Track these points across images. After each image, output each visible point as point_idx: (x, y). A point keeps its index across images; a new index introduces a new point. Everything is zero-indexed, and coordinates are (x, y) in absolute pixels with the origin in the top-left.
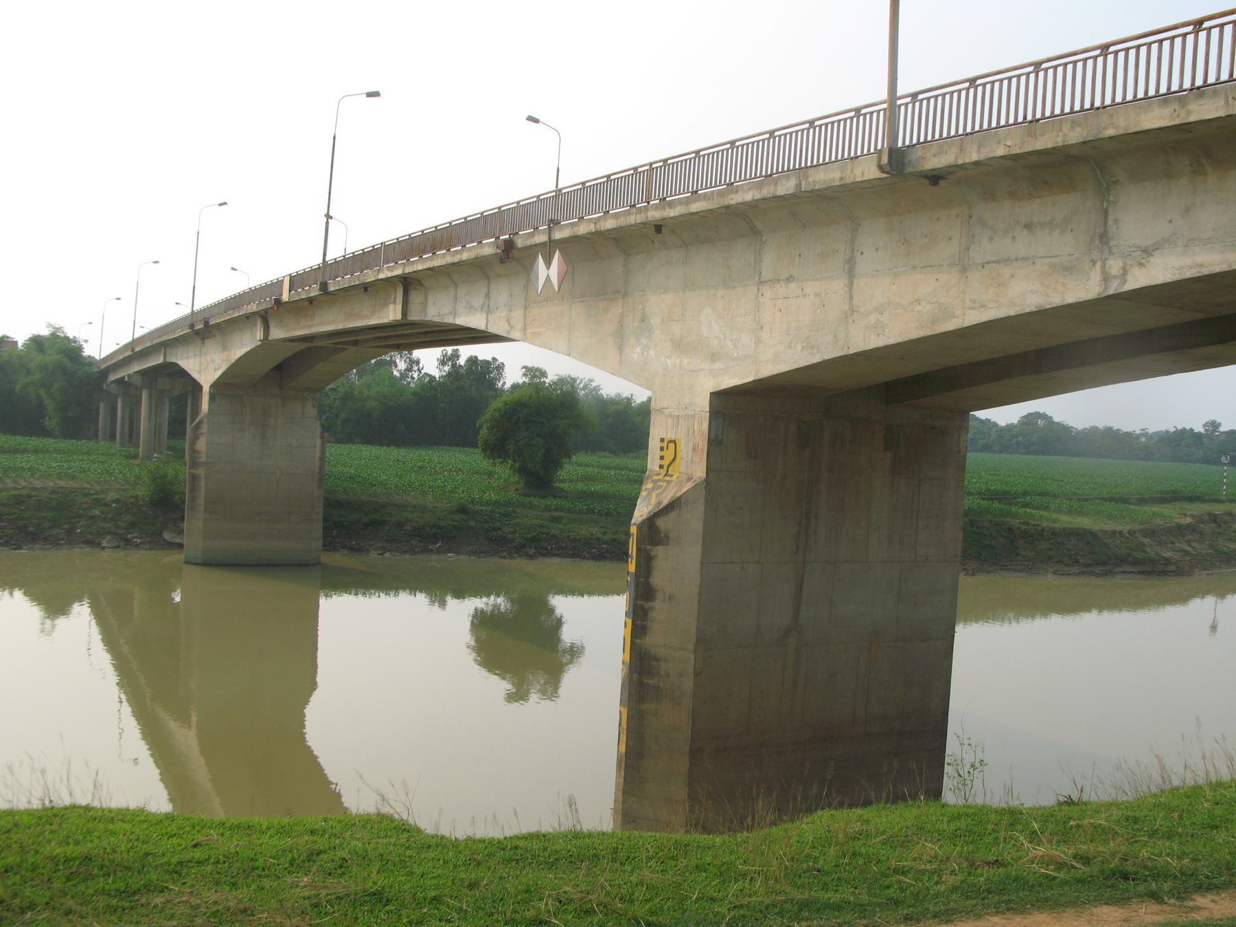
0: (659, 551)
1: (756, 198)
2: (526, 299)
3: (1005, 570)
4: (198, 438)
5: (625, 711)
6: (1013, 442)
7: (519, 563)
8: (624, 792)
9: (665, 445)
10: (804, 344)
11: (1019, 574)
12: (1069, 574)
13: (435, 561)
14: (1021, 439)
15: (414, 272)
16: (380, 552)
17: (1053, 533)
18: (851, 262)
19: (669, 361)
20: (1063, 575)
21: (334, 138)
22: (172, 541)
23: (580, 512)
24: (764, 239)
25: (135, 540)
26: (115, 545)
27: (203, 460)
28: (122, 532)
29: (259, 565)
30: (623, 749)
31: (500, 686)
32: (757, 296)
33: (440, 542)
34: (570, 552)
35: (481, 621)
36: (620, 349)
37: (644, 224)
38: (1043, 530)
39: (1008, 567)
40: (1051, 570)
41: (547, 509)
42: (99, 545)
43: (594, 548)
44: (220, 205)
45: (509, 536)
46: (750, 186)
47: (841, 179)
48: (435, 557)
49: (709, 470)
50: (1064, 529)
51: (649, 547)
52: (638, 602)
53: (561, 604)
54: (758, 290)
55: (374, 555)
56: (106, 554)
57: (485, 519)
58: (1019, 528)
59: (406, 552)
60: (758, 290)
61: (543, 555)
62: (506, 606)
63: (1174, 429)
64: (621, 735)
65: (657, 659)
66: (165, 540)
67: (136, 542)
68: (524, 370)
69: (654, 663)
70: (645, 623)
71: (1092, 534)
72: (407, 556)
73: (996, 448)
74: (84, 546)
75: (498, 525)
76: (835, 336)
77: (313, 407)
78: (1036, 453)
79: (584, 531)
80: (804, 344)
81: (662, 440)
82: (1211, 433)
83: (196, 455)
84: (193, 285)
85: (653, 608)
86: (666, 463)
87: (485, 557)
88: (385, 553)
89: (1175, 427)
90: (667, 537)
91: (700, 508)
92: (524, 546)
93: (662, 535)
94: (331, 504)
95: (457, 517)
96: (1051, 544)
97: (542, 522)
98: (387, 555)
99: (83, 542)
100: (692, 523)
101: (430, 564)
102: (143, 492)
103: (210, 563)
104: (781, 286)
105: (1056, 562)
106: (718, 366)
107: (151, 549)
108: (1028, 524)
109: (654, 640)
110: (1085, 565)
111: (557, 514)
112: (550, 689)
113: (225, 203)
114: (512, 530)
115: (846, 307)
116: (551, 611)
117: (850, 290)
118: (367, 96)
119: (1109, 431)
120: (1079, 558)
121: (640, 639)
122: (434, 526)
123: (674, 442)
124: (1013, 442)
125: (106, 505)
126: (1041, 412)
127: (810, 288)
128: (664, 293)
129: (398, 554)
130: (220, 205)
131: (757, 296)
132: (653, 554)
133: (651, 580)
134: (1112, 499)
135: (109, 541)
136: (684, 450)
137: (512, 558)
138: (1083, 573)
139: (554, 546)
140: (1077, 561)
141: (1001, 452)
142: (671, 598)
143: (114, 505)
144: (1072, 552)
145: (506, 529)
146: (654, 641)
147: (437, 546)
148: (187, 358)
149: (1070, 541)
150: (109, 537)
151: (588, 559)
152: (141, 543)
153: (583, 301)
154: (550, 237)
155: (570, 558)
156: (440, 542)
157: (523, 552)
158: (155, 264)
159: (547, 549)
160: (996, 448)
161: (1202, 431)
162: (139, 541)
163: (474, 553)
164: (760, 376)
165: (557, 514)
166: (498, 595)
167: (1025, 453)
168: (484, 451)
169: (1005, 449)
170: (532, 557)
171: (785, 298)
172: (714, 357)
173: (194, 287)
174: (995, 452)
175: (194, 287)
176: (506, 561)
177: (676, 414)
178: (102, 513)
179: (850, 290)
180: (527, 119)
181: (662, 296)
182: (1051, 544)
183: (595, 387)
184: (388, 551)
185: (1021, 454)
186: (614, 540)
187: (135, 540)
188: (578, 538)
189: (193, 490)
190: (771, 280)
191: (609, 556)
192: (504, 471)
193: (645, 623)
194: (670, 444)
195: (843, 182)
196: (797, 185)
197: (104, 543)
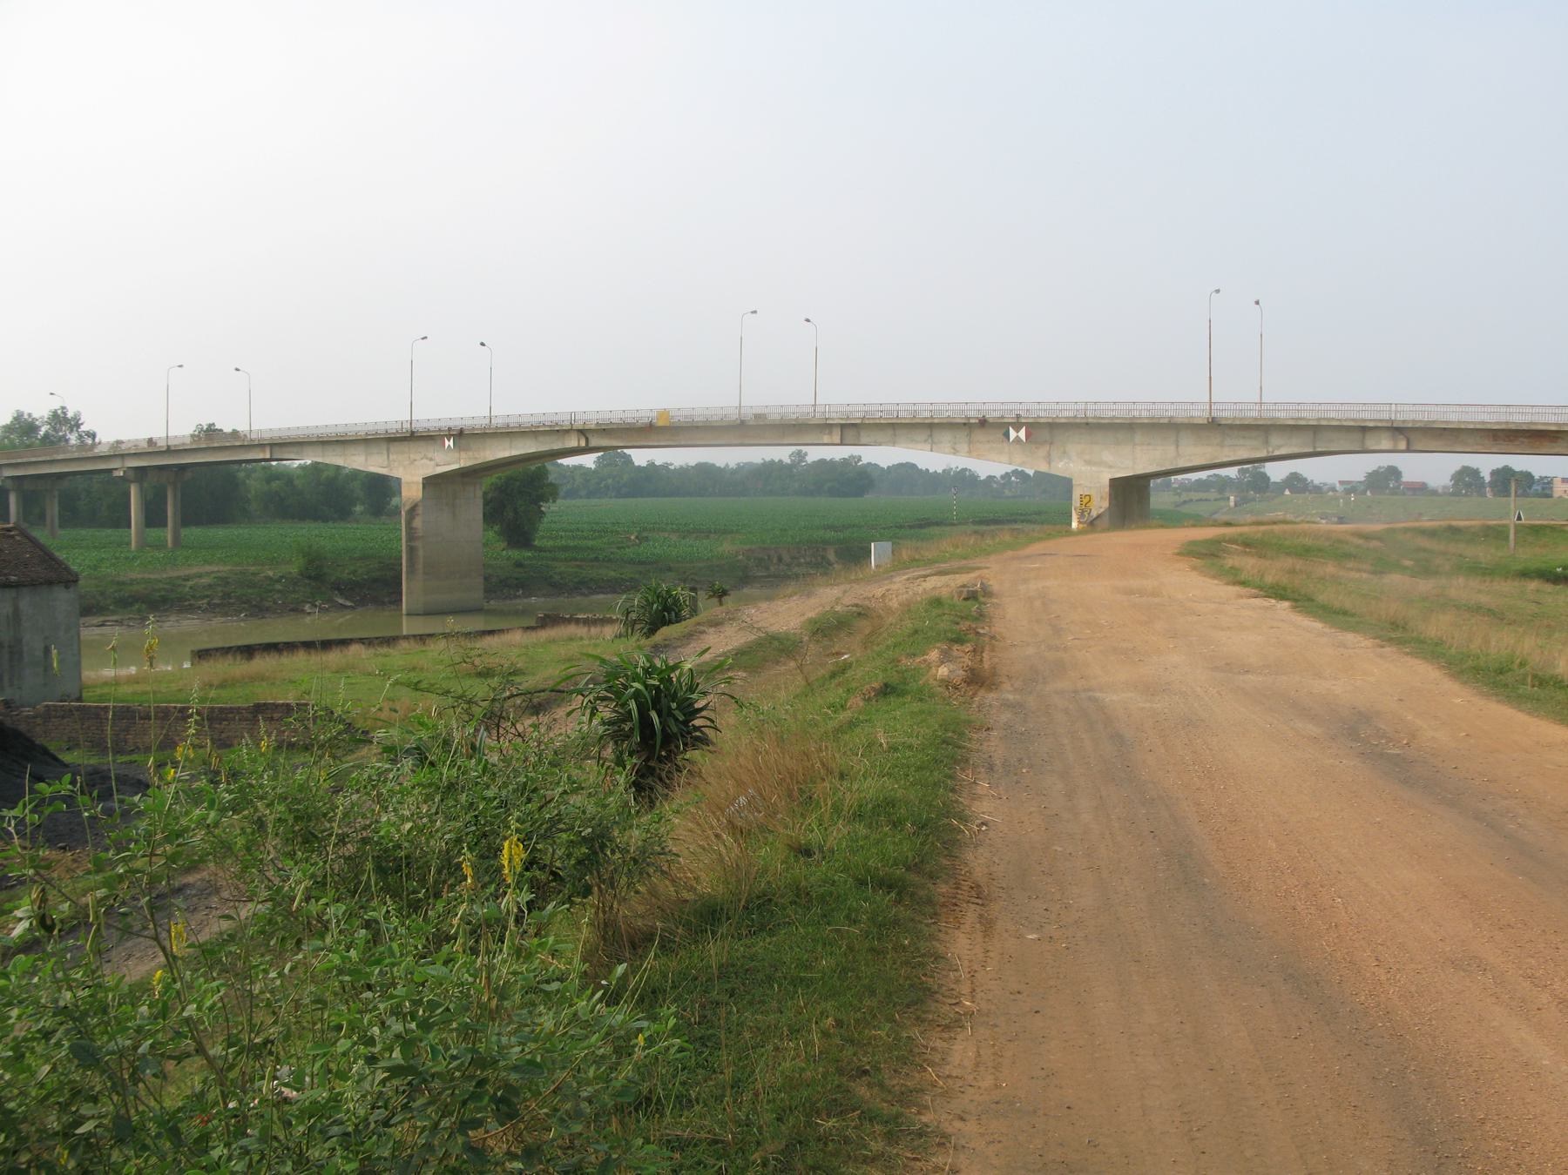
14: (610, 481)
18: (1177, 441)
113: (426, 338)
141: (590, 495)
160: (583, 493)
161: (789, 461)
172: (1111, 467)
174: (581, 497)
185: (611, 497)
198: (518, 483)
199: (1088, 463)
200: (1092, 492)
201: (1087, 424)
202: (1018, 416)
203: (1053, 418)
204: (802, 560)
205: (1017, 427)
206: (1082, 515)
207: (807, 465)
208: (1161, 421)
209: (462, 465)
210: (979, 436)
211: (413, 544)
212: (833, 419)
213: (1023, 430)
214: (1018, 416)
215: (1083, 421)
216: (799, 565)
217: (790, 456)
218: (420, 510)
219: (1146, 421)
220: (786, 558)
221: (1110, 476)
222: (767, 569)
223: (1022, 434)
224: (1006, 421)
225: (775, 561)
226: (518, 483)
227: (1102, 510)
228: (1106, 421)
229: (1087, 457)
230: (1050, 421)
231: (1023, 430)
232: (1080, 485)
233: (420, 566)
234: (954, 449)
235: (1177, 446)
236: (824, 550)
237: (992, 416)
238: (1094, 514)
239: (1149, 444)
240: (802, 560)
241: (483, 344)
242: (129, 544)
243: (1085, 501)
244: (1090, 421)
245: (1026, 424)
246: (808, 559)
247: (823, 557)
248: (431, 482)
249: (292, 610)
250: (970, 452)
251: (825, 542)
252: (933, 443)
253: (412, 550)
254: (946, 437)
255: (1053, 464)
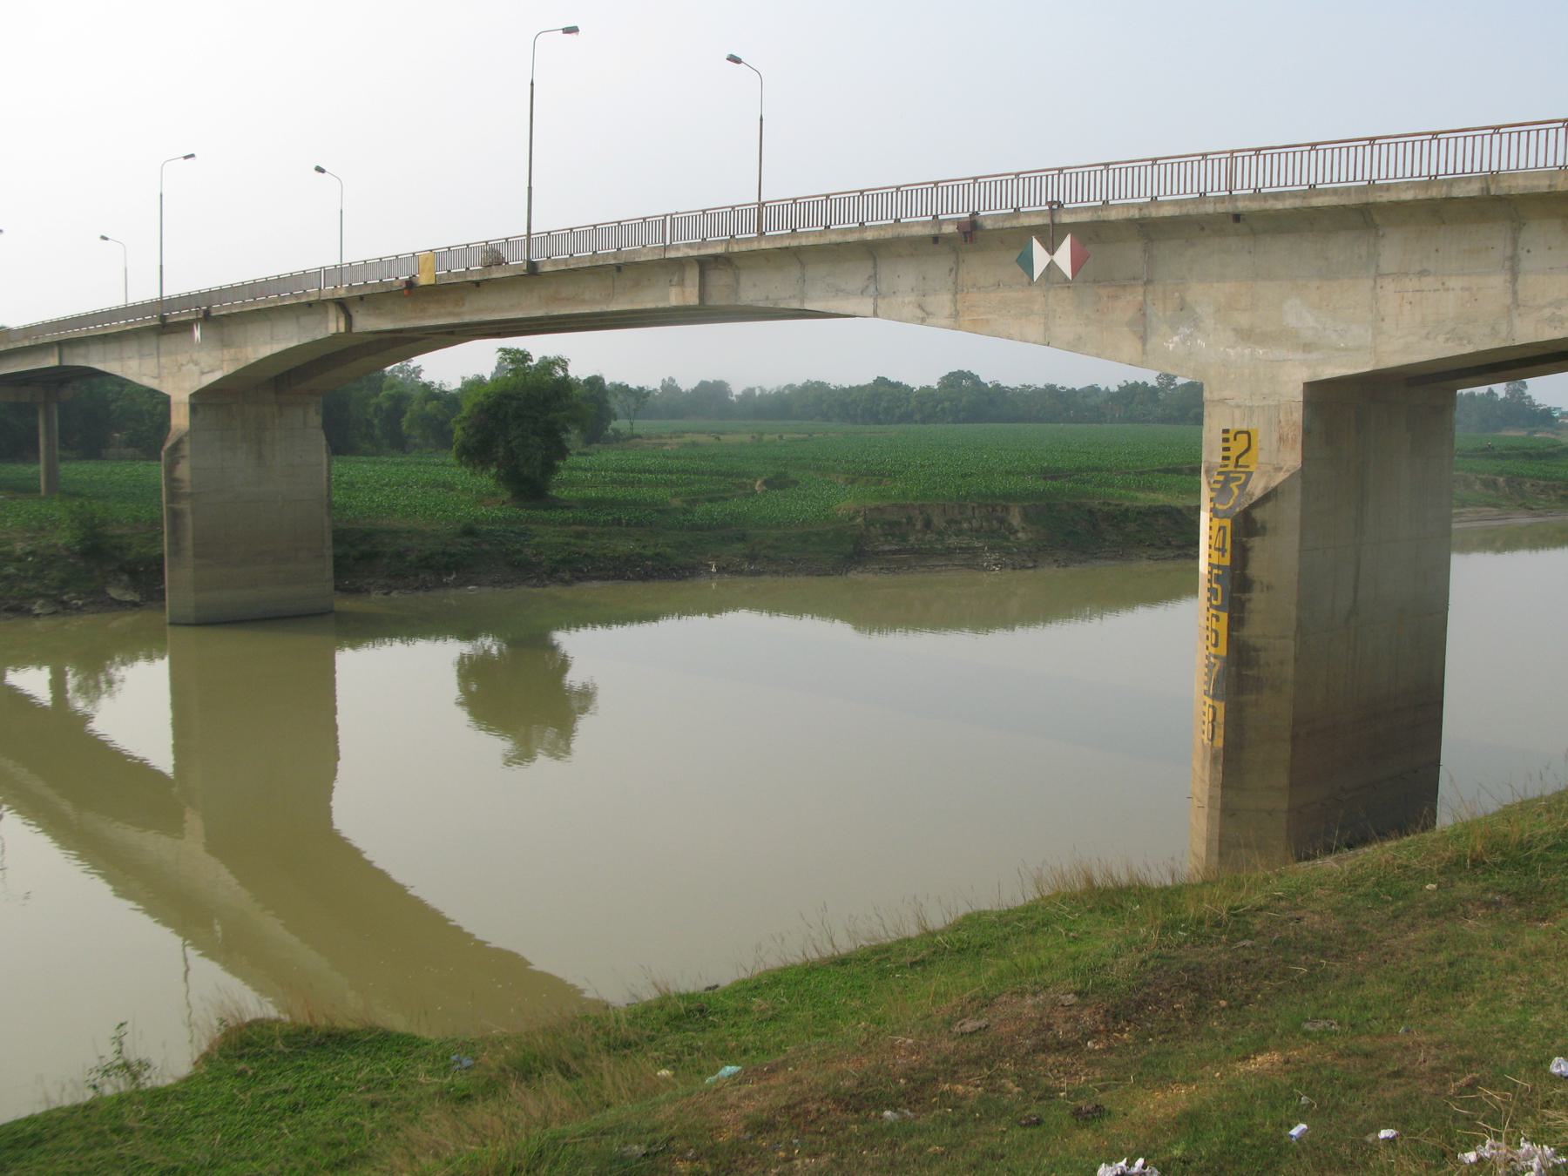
0: (1256, 543)
1: (1420, 197)
2: (955, 283)
3: (1096, 558)
4: (178, 463)
5: (1221, 707)
6: (938, 409)
7: (554, 590)
8: (1223, 787)
9: (1231, 436)
10: (1448, 336)
11: (1113, 562)
12: (1165, 559)
13: (452, 597)
14: (947, 404)
15: (752, 251)
16: (385, 591)
17: (1140, 513)
18: (1514, 259)
19: (1231, 352)
20: (1158, 559)
21: (532, 84)
22: (122, 598)
23: (606, 523)
24: (1381, 233)
25: (75, 602)
26: (51, 612)
27: (188, 490)
28: (55, 592)
29: (265, 619)
30: (1219, 742)
31: (496, 745)
32: (1374, 288)
33: (454, 573)
34: (611, 573)
35: (469, 670)
36: (1144, 339)
37: (1226, 214)
38: (1127, 510)
39: (1098, 555)
40: (1144, 555)
41: (564, 523)
42: (29, 612)
43: (638, 566)
44: (186, 157)
45: (534, 559)
46: (1409, 185)
47: (1550, 186)
48: (453, 592)
49: (1304, 459)
50: (1150, 507)
51: (1244, 539)
52: (1234, 595)
53: (569, 641)
54: (1375, 282)
55: (376, 596)
56: (38, 624)
57: (499, 541)
58: (1100, 510)
59: (417, 589)
60: (1375, 282)
61: (579, 579)
62: (499, 650)
63: (1125, 384)
64: (1216, 730)
65: (1256, 650)
66: (112, 599)
67: (76, 604)
68: (500, 353)
69: (1253, 653)
70: (1242, 615)
71: (1179, 511)
72: (421, 594)
73: (917, 417)
74: (11, 615)
75: (518, 546)
76: (1493, 328)
77: (317, 414)
78: (965, 421)
79: (625, 546)
80: (1448, 336)
81: (1226, 431)
82: (1166, 387)
83: (175, 484)
84: (159, 264)
85: (1250, 600)
86: (1233, 454)
87: (512, 587)
88: (391, 592)
89: (1125, 381)
90: (1264, 528)
91: (1297, 497)
92: (555, 570)
93: (1259, 526)
94: (339, 537)
95: (466, 540)
96: (1138, 525)
97: (567, 539)
98: (394, 594)
99: (6, 610)
100: (1290, 512)
101: (445, 601)
102: (63, 538)
103: (207, 621)
104: (1411, 280)
105: (1148, 546)
106: (1314, 356)
107: (98, 612)
108: (1109, 504)
109: (1254, 631)
110: (1179, 547)
111: (580, 528)
112: (562, 743)
113: (192, 156)
114: (535, 552)
115: (1508, 301)
116: (554, 649)
117: (1514, 286)
118: (564, 33)
119: (1051, 389)
120: (1170, 539)
121: (1237, 631)
122: (444, 553)
123: (1248, 433)
124: (938, 409)
125: (19, 559)
126: (966, 371)
127: (1455, 283)
128: (1218, 282)
129: (408, 592)
130: (186, 157)
131: (1374, 288)
132: (1249, 545)
133: (1247, 572)
134: (1167, 471)
135: (42, 606)
136: (1265, 443)
137: (545, 586)
138: (1178, 556)
139: (590, 567)
140: (1169, 543)
141: (924, 421)
142: (1269, 587)
143: (30, 559)
144: (1162, 533)
145: (528, 552)
146: (1254, 631)
147: (452, 578)
148: (142, 356)
149: (1157, 521)
150: (40, 602)
151: (633, 580)
152: (83, 605)
153: (1069, 287)
154: (1052, 221)
155: (612, 580)
156: (454, 573)
157: (555, 578)
158: (107, 236)
159: (583, 572)
160: (917, 417)
161: (1156, 384)
162: (80, 603)
163: (494, 583)
164: (1382, 366)
165: (580, 528)
166: (487, 636)
167: (955, 422)
168: (459, 456)
169: (906, 418)
170: (567, 583)
171: (1418, 291)
172: (1307, 347)
173: (161, 266)
174: (916, 422)
175: (161, 266)
176: (535, 590)
177: (1248, 403)
178: (18, 569)
179: (1514, 286)
180: (728, 59)
181: (1216, 285)
182: (1138, 525)
183: (414, 368)
184: (395, 589)
185: (948, 423)
186: (658, 554)
187: (75, 602)
188: (617, 555)
189: (175, 530)
190: (1395, 274)
191: (656, 574)
192: (485, 480)
193: (1242, 615)
194: (1238, 436)
195: (1553, 190)
196: (1482, 189)
197: (37, 609)
198: (514, 403)
199: (1246, 335)
200: (1257, 425)
201: (1237, 217)
202: (1055, 207)
203: (1141, 207)
204: (965, 525)
205: (1051, 235)
206: (1223, 490)
207: (1176, 388)
208: (1458, 192)
209: (226, 373)
210: (977, 268)
211: (175, 506)
212: (677, 248)
213: (1066, 245)
214: (1055, 207)
215: (1221, 208)
216: (959, 533)
217: (1157, 378)
218: (186, 449)
219: (1408, 196)
220: (939, 522)
221: (1305, 375)
222: (904, 538)
223: (1063, 257)
224: (1025, 222)
225: (919, 526)
226: (514, 403)
227: (1280, 477)
228: (1288, 204)
229: (1243, 320)
230: (1135, 213)
231: (1066, 245)
232: (1223, 401)
233: (188, 543)
234: (921, 307)
235: (1514, 274)
236: (1006, 509)
237: (992, 210)
238: (1257, 487)
239: (1423, 273)
240: (965, 525)
241: (320, 170)
242: (39, 491)
243: (1238, 446)
244: (1241, 206)
245: (1075, 229)
246: (975, 524)
247: (1002, 521)
248: (203, 400)
249: (12, 610)
250: (956, 315)
251: (1009, 497)
252: (878, 295)
253: (176, 515)
254: (903, 277)
255: (1154, 341)
